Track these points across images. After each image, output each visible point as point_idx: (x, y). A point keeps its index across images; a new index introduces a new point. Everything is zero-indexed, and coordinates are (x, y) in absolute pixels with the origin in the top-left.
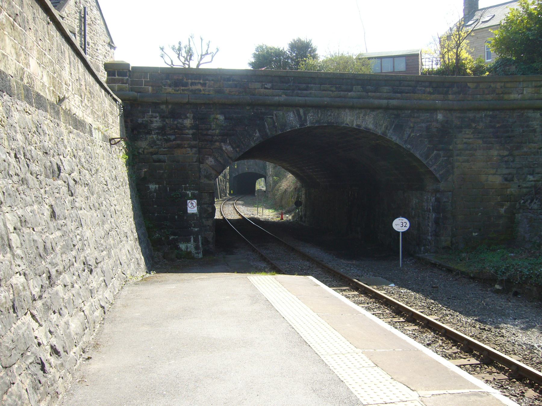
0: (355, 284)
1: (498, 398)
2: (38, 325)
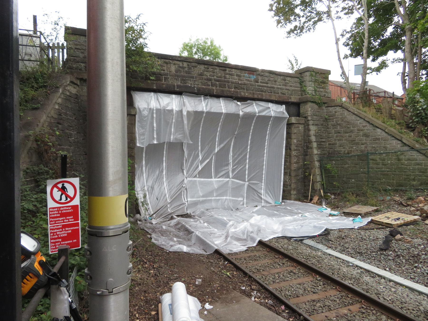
0: (313, 194)
1: (335, 45)
2: (341, 72)
